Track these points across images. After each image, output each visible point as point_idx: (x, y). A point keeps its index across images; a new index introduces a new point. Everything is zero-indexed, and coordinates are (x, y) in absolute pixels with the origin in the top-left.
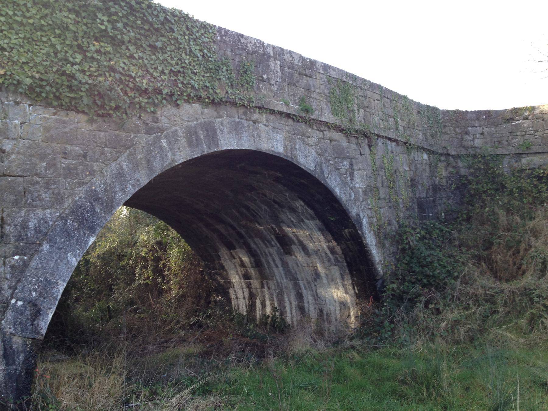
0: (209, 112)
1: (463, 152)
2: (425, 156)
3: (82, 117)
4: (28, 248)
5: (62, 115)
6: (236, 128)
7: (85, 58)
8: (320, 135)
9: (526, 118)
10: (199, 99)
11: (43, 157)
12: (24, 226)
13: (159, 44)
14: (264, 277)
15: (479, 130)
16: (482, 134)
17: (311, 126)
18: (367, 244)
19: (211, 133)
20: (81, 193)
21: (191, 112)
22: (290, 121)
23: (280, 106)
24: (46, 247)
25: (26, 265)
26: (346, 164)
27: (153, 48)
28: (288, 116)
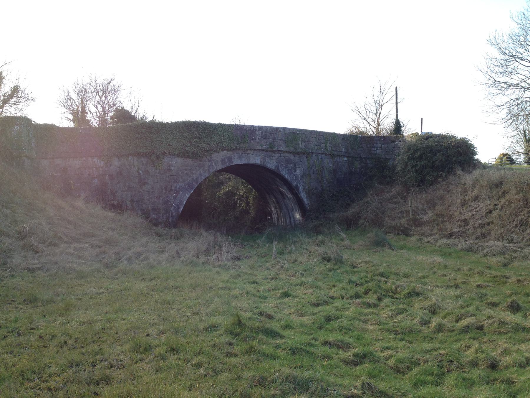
0: (230, 153)
1: (370, 156)
2: (345, 159)
3: (191, 160)
4: (177, 192)
5: (185, 160)
6: (240, 157)
7: (191, 144)
8: (279, 155)
9: (400, 141)
10: (226, 150)
11: (180, 171)
12: (176, 187)
13: (213, 136)
14: (280, 208)
15: (379, 145)
16: (381, 147)
17: (275, 153)
18: (301, 197)
19: (230, 159)
20: (190, 179)
21: (224, 154)
22: (264, 152)
23: (259, 147)
24: (181, 192)
25: (176, 197)
26: (292, 166)
27: (211, 138)
28: (263, 150)
